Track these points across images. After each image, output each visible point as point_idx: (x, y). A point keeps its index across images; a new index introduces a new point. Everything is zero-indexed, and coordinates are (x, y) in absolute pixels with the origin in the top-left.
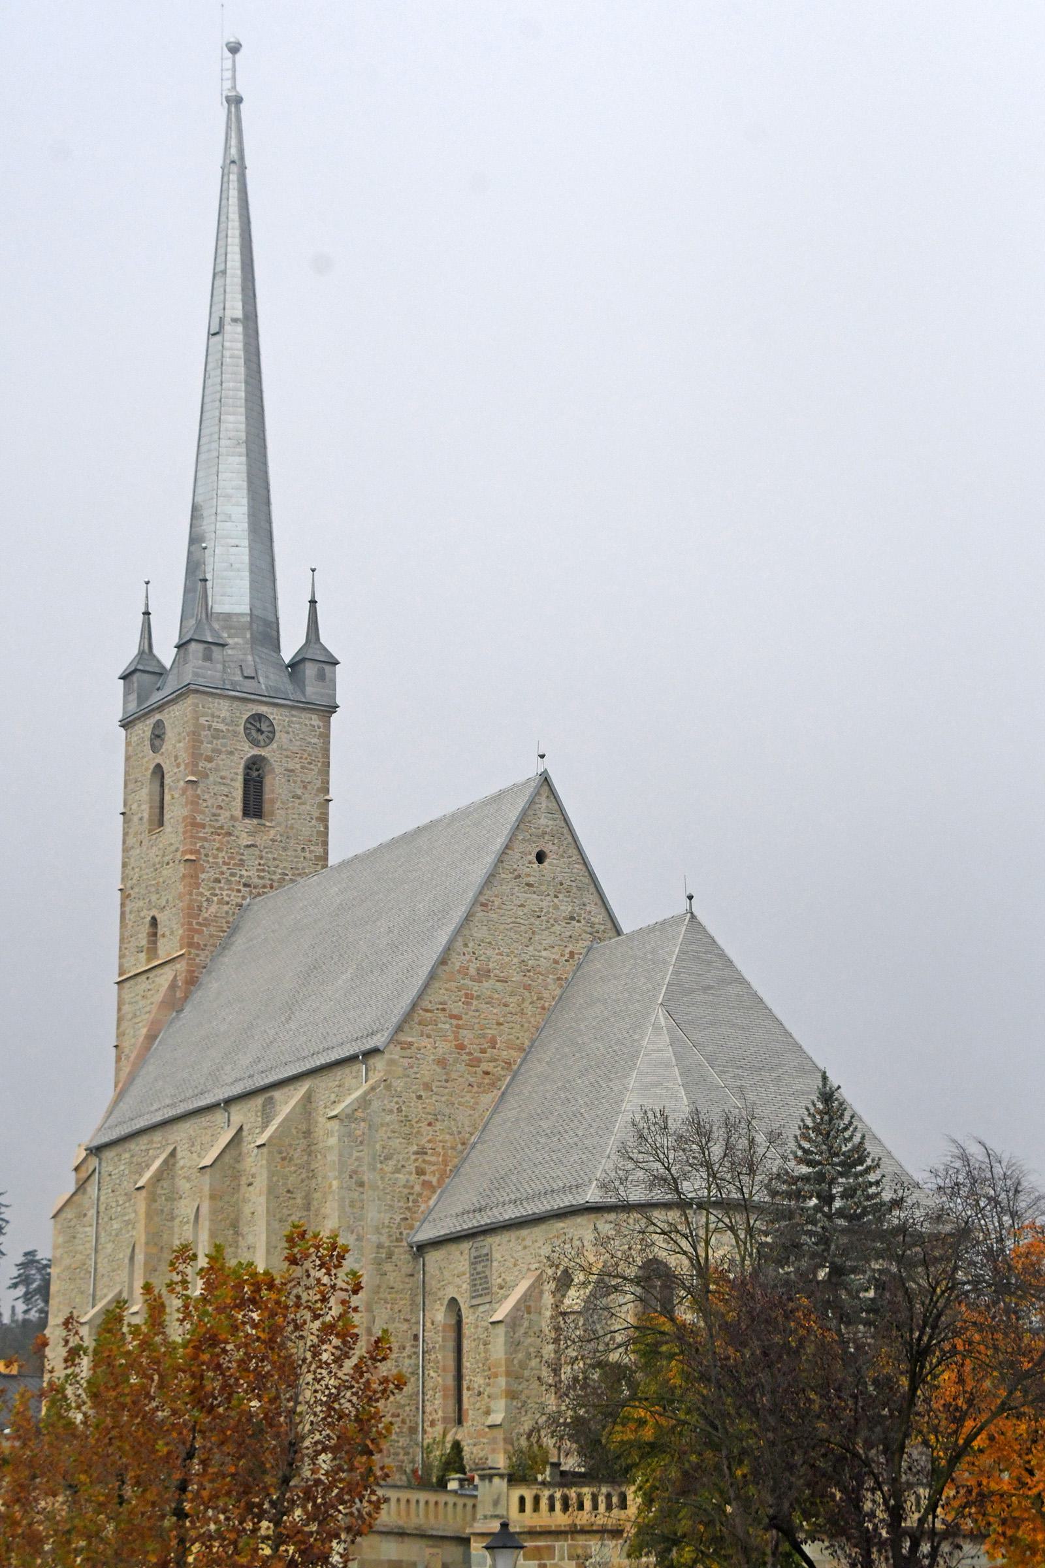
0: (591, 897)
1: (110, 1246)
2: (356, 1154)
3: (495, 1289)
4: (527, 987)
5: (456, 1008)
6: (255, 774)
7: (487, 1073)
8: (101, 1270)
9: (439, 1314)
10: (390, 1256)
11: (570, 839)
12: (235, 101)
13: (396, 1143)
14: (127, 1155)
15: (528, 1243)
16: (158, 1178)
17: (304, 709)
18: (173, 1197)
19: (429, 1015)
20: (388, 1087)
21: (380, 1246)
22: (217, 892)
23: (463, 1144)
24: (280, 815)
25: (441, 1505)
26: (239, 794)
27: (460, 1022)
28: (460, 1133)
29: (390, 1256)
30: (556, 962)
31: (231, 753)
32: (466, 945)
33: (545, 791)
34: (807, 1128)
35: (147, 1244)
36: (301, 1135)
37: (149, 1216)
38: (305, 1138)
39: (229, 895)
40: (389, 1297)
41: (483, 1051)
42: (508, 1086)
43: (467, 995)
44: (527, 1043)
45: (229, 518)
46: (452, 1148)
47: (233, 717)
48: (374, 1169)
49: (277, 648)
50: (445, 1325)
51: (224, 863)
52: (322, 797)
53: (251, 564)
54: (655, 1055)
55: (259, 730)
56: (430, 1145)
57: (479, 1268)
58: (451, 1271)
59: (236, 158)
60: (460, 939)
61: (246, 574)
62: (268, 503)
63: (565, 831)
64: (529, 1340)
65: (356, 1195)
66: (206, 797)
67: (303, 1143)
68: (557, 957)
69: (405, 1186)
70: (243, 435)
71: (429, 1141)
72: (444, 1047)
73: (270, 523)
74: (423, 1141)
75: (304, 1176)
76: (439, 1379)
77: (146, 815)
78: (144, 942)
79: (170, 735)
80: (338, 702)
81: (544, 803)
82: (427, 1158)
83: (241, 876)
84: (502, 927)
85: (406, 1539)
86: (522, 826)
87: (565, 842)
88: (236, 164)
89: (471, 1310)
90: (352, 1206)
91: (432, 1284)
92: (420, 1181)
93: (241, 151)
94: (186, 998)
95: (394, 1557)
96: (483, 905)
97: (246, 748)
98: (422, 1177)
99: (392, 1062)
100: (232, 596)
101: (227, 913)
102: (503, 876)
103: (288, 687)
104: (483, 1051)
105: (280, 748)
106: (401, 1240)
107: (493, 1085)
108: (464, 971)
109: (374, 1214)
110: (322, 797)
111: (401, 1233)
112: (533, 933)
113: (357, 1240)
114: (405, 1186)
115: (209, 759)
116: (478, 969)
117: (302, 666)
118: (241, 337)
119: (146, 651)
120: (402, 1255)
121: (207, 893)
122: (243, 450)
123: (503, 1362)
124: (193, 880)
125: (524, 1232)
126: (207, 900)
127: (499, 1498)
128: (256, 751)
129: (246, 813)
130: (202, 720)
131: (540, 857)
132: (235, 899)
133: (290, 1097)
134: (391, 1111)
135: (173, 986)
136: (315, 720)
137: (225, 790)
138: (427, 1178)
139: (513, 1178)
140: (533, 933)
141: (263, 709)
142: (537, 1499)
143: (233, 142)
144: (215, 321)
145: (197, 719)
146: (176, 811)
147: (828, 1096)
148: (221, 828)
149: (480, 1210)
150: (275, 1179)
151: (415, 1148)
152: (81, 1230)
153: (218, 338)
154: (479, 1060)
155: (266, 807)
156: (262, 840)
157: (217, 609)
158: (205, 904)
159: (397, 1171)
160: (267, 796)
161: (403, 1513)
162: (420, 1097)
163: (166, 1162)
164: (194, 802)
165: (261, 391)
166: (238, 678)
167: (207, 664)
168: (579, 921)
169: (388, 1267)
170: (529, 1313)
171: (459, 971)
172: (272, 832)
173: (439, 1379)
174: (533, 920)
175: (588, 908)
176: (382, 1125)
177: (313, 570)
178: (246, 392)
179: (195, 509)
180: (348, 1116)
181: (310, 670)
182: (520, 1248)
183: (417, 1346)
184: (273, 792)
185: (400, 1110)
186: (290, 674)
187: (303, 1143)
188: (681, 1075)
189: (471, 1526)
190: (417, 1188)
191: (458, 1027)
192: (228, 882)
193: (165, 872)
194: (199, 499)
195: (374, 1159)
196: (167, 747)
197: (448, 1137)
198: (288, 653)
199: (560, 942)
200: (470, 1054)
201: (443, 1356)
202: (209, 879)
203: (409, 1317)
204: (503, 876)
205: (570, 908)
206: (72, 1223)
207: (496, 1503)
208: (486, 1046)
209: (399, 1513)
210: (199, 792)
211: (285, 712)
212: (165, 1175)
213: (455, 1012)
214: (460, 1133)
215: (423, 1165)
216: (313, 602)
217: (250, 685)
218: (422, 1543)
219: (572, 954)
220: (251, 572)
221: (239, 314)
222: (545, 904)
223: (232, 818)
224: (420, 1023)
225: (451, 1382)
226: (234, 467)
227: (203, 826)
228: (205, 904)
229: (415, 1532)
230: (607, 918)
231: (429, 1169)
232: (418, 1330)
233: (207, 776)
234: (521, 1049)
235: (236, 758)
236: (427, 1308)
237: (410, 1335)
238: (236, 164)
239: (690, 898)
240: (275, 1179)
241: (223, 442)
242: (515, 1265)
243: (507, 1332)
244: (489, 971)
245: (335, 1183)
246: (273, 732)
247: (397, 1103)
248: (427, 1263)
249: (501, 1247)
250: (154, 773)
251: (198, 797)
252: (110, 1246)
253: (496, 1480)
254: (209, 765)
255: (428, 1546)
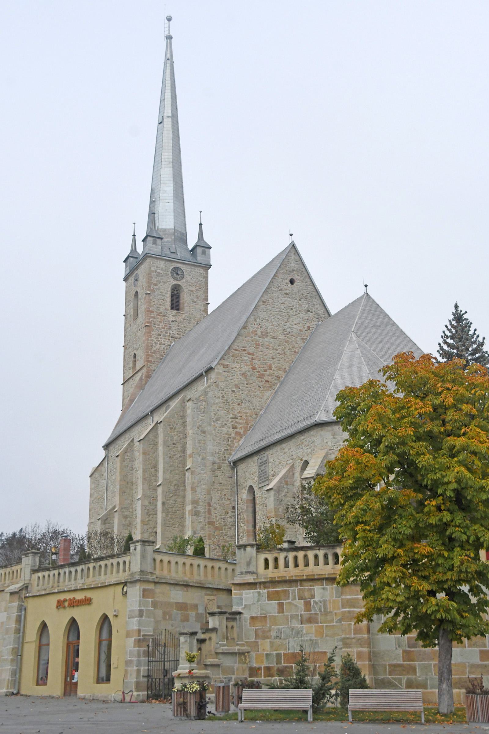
0: (317, 302)
1: (112, 487)
2: (201, 418)
3: (270, 477)
4: (287, 342)
5: (252, 350)
6: (176, 292)
7: (268, 381)
8: (108, 498)
9: (244, 495)
10: (219, 468)
11: (306, 274)
12: (169, 38)
13: (222, 413)
14: (117, 446)
15: (286, 450)
16: (126, 451)
17: (197, 266)
18: (132, 460)
19: (238, 352)
20: (217, 386)
21: (214, 463)
22: (160, 339)
23: (256, 414)
24: (187, 309)
25: (216, 569)
26: (169, 299)
27: (254, 357)
28: (254, 409)
29: (219, 468)
30: (301, 331)
31: (165, 282)
32: (255, 320)
33: (293, 251)
34: (447, 337)
35: (121, 480)
36: (180, 418)
37: (122, 468)
38: (182, 419)
39: (165, 341)
40: (219, 488)
41: (265, 371)
42: (279, 388)
43: (256, 344)
44: (287, 368)
45: (165, 192)
46: (251, 416)
47: (166, 269)
48: (211, 425)
49: (186, 243)
50: (247, 500)
51: (162, 328)
52: (205, 302)
53: (174, 209)
54: (350, 353)
55: (177, 274)
56: (239, 415)
57: (263, 468)
58: (249, 472)
59: (169, 58)
60: (253, 317)
61: (172, 214)
62: (182, 187)
63: (304, 270)
64: (287, 499)
65: (201, 438)
66: (154, 300)
67: (181, 421)
68: (301, 328)
69: (226, 434)
70: (171, 160)
71: (238, 413)
72: (245, 368)
73: (183, 195)
74: (236, 412)
75: (181, 437)
76: (245, 527)
77: (132, 313)
78: (131, 365)
79: (141, 278)
80: (211, 264)
81: (293, 256)
82: (237, 420)
83: (170, 334)
84: (273, 313)
85: (190, 589)
86: (282, 266)
87: (304, 275)
88: (169, 60)
89: (259, 490)
90: (199, 443)
91: (241, 480)
92: (234, 432)
93: (172, 56)
94: (146, 383)
95: (181, 601)
96: (263, 302)
97: (172, 281)
98: (235, 430)
99: (218, 374)
100: (166, 222)
101: (164, 348)
102: (273, 289)
103: (191, 258)
104: (265, 371)
105: (187, 281)
106: (225, 460)
107: (271, 387)
108: (255, 332)
109: (211, 447)
110: (205, 302)
111: (225, 457)
112: (289, 316)
113: (202, 459)
114: (226, 434)
115: (156, 285)
116: (262, 332)
117: (195, 250)
118: (171, 123)
119: (134, 249)
120: (226, 468)
121: (155, 340)
122: (171, 165)
123: (273, 510)
124: (149, 334)
125: (284, 445)
126: (155, 343)
127: (250, 560)
128: (176, 282)
129: (172, 308)
130: (152, 269)
131: (292, 282)
132: (167, 343)
133: (174, 402)
134: (219, 397)
135: (141, 379)
136: (202, 271)
137: (163, 298)
138: (238, 430)
139: (279, 422)
140: (289, 316)
141: (179, 265)
142: (276, 560)
143: (168, 52)
144: (161, 117)
145: (150, 268)
146: (142, 309)
147: (458, 317)
148: (161, 313)
149: (263, 440)
150: (167, 438)
151: (231, 416)
152: (101, 481)
153: (162, 125)
154: (263, 375)
155: (181, 306)
156: (179, 319)
157: (160, 227)
158: (154, 344)
159: (223, 426)
160: (181, 301)
161: (188, 573)
162: (233, 391)
163: (129, 444)
164: (149, 302)
165: (179, 144)
166: (168, 253)
167: (154, 246)
168: (311, 312)
169: (218, 473)
170: (287, 484)
171: (252, 332)
172: (184, 316)
173: (245, 527)
174: (289, 311)
175: (316, 307)
176: (214, 404)
177: (201, 212)
178: (173, 143)
179: (152, 190)
180: (196, 399)
181: (199, 250)
182: (282, 454)
183: (235, 512)
184: (183, 299)
185: (223, 397)
186: (192, 254)
187: (181, 421)
188: (365, 361)
189: (233, 579)
190: (233, 435)
191: (252, 359)
192: (165, 336)
193: (138, 334)
194: (153, 186)
195: (210, 420)
196: (139, 283)
197: (248, 411)
198: (190, 246)
199: (302, 322)
200: (259, 372)
201: (247, 516)
202: (156, 334)
203: (230, 498)
204: (273, 289)
205: (307, 306)
206: (98, 479)
207: (249, 564)
208: (267, 368)
209: (185, 573)
210: (151, 298)
211: (188, 267)
212: (129, 450)
213: (251, 351)
214: (254, 409)
215: (236, 424)
216: (201, 224)
217: (173, 256)
218: (204, 592)
219: (309, 327)
220: (174, 212)
221: (170, 115)
222: (294, 303)
223: (166, 309)
224: (233, 356)
225: (251, 528)
226: (167, 174)
227: (153, 312)
228: (154, 344)
229: (196, 585)
230: (325, 312)
231: (239, 426)
232: (235, 504)
233: (154, 292)
234: (284, 371)
235: (167, 284)
236: (239, 493)
237: (230, 506)
238: (169, 60)
239: (366, 286)
240: (167, 438)
241: (163, 163)
242: (280, 463)
243: (275, 495)
244: (268, 333)
245: (190, 432)
246: (184, 275)
247: (222, 393)
248: (238, 471)
249: (273, 455)
250: (135, 295)
251: (151, 300)
252: (112, 487)
253: (249, 549)
254: (155, 287)
255: (206, 595)
